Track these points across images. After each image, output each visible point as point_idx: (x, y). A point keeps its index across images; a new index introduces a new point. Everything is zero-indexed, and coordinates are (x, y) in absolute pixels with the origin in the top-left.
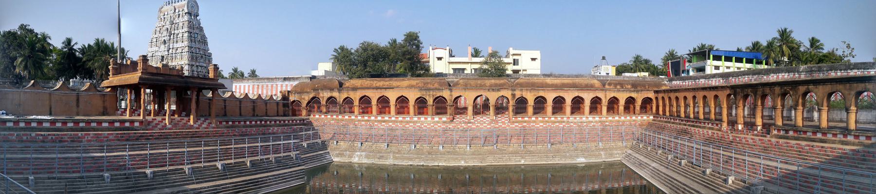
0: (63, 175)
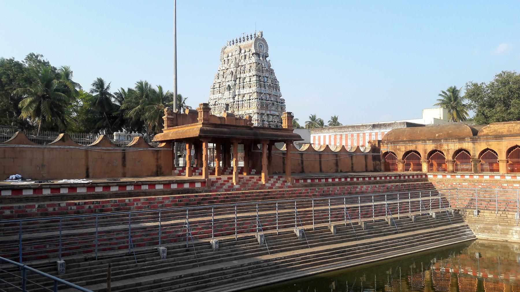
0: (105, 254)
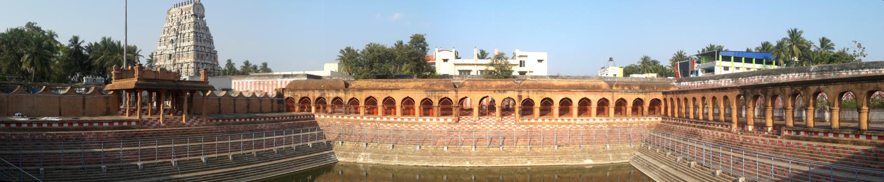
0: (68, 167)
